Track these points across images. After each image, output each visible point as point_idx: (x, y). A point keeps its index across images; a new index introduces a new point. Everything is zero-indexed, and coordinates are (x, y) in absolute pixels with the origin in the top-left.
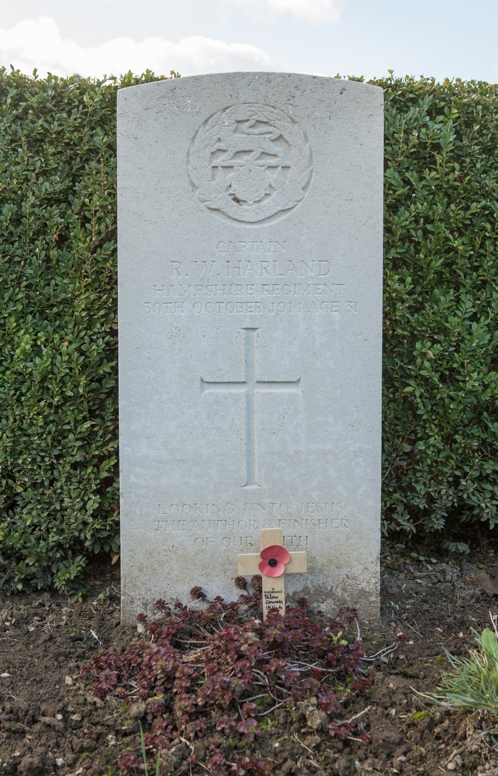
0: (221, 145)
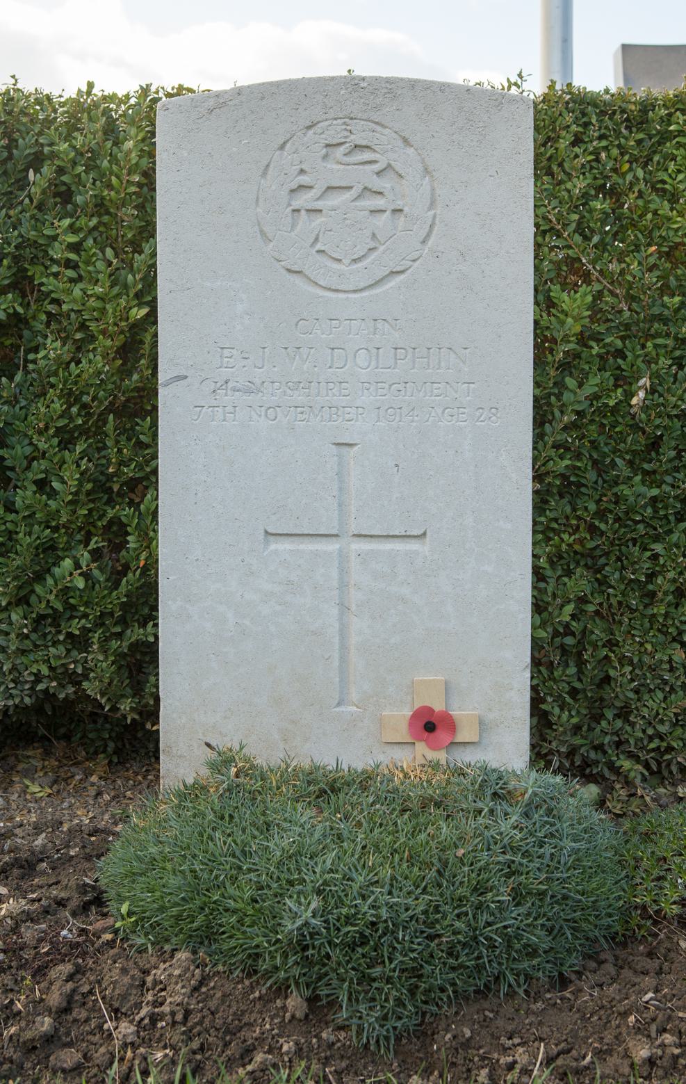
0: (304, 179)
